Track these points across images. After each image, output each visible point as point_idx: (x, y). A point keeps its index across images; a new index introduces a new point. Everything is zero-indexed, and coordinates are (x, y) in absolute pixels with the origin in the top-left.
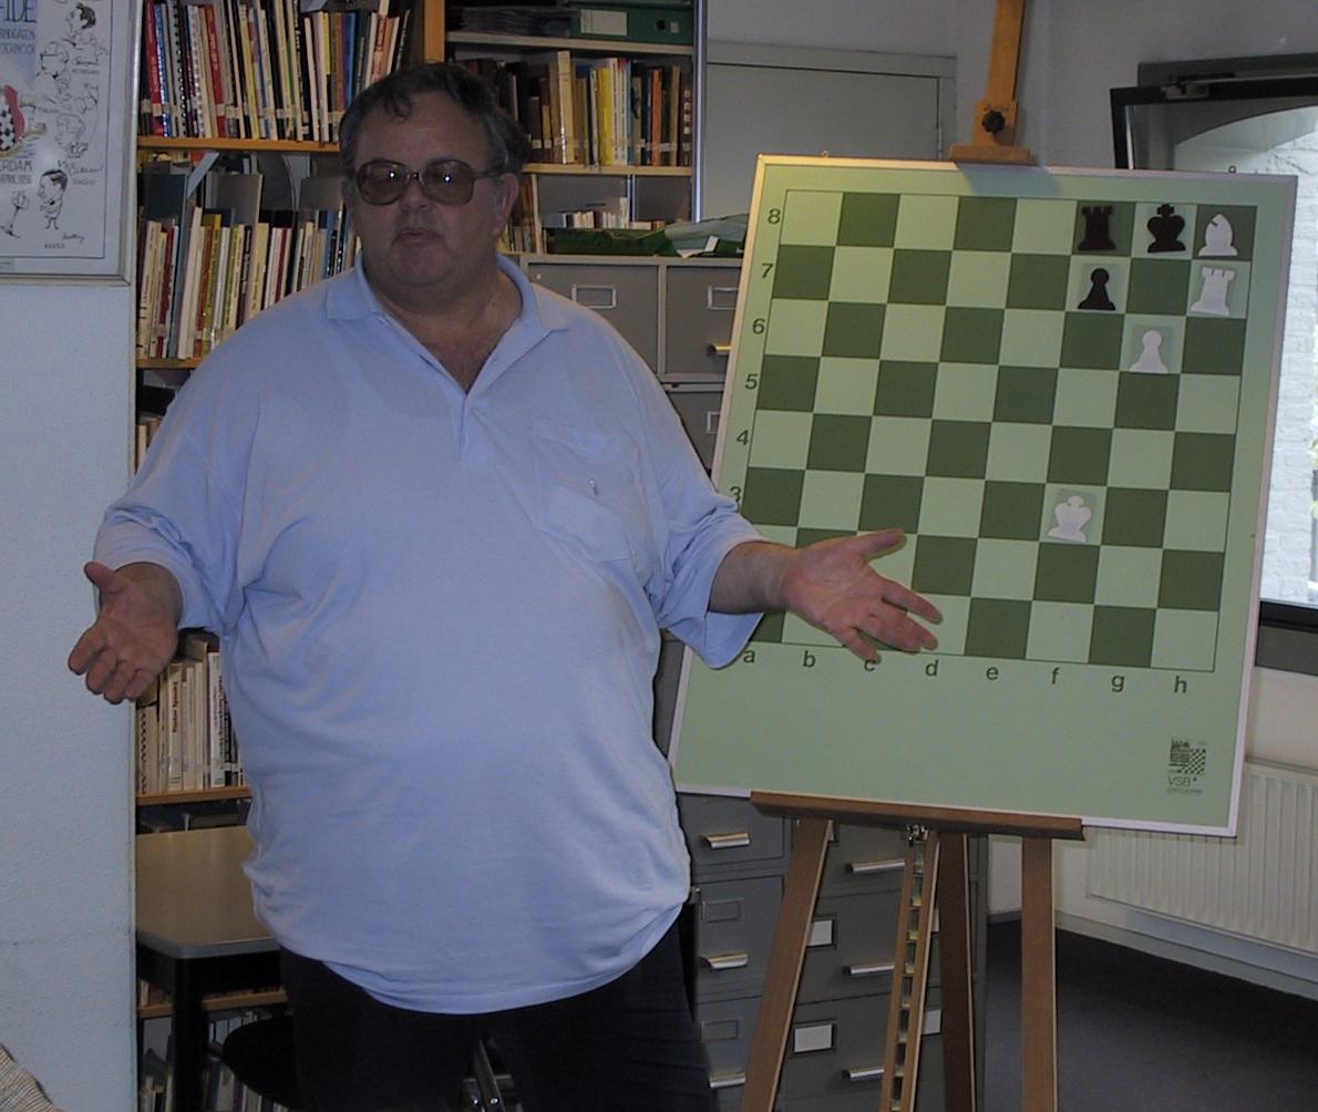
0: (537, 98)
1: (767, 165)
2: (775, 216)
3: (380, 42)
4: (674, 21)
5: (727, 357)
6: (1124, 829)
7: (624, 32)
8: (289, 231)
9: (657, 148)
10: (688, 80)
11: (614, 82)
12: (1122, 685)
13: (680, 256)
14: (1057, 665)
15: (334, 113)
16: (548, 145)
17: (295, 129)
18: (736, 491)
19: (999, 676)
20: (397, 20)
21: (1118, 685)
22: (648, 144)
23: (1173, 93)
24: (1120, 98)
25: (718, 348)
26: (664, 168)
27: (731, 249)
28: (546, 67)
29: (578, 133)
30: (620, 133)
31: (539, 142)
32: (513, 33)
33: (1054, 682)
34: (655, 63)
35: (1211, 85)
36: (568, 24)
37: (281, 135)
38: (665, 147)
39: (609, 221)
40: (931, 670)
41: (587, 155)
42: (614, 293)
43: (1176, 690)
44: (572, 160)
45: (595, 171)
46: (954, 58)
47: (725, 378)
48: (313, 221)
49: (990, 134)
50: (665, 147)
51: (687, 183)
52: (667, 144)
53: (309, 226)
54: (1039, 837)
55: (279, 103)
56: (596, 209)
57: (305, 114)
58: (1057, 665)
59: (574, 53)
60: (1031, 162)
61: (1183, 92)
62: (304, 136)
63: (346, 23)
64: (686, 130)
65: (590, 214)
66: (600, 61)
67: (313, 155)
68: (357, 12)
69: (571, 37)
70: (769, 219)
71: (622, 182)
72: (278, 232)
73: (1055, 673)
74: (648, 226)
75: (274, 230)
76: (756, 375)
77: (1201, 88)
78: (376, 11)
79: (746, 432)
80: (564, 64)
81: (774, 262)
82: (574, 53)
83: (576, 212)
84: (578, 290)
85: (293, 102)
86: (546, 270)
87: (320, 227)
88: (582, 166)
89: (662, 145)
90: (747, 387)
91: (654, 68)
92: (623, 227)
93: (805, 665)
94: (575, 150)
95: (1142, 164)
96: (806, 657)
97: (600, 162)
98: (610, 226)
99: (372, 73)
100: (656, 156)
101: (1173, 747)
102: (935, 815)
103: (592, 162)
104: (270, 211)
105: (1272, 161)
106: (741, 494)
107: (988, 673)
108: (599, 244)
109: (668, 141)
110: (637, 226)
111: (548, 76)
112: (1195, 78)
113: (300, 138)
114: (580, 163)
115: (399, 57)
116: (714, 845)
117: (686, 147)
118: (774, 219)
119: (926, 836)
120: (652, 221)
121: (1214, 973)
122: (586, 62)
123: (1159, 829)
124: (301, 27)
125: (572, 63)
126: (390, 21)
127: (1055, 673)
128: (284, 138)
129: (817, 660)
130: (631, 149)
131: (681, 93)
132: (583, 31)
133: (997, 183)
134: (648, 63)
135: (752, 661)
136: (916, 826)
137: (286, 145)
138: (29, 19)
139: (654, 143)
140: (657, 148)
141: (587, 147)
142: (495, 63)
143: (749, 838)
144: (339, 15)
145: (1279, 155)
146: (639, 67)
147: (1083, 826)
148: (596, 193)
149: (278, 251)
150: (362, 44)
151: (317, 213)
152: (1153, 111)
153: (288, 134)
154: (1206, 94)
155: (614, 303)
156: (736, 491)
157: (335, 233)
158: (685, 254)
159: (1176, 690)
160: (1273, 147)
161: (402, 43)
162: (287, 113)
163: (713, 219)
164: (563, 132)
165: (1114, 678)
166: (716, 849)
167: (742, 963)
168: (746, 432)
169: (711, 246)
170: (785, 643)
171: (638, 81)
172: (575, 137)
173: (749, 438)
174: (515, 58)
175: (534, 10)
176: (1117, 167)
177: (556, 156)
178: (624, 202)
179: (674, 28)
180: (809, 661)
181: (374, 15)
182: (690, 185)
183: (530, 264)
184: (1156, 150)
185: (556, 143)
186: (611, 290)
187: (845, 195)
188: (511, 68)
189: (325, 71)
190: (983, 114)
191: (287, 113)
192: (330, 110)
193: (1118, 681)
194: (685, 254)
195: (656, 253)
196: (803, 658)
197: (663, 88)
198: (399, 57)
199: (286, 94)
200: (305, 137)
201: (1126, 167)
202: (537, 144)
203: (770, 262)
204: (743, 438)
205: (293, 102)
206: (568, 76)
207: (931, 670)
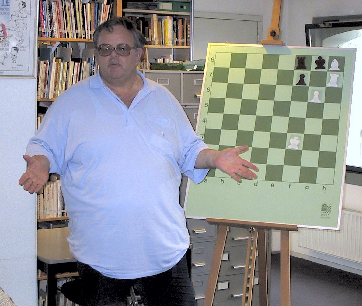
2: (213, 60)
8: (79, 64)
9: (180, 41)
10: (189, 22)
11: (169, 22)
12: (308, 189)
16: (150, 40)
18: (202, 135)
20: (109, 5)
22: (178, 40)
23: (322, 25)
24: (307, 27)
25: (197, 96)
27: (201, 69)
29: (159, 37)
30: (170, 36)
31: (148, 39)
32: (141, 9)
33: (289, 188)
35: (332, 24)
36: (156, 6)
37: (77, 37)
38: (183, 40)
39: (167, 61)
40: (256, 184)
41: (162, 43)
42: (169, 81)
43: (323, 190)
45: (164, 47)
46: (262, 16)
47: (199, 104)
49: (272, 37)
50: (183, 40)
51: (189, 50)
53: (85, 62)
54: (285, 230)
55: (77, 28)
56: (164, 57)
57: (84, 31)
59: (158, 15)
60: (283, 44)
62: (84, 37)
63: (95, 6)
65: (162, 59)
67: (86, 43)
68: (98, 3)
72: (76, 64)
74: (178, 62)
75: (75, 63)
76: (208, 103)
77: (330, 24)
79: (205, 119)
81: (213, 72)
83: (158, 58)
84: (159, 80)
85: (81, 28)
86: (150, 74)
87: (88, 62)
88: (160, 46)
94: (158, 41)
95: (314, 45)
96: (221, 181)
99: (102, 20)
100: (180, 43)
102: (257, 224)
103: (163, 45)
106: (204, 136)
110: (175, 62)
112: (328, 21)
113: (82, 38)
114: (159, 45)
116: (196, 233)
117: (188, 41)
118: (213, 60)
119: (254, 230)
122: (161, 16)
124: (83, 7)
125: (157, 17)
126: (107, 6)
129: (224, 181)
130: (173, 41)
132: (160, 9)
133: (274, 50)
134: (178, 17)
135: (207, 182)
137: (78, 40)
141: (161, 40)
144: (93, 4)
146: (176, 18)
147: (297, 227)
148: (164, 53)
150: (99, 12)
152: (317, 30)
153: (79, 37)
155: (169, 84)
157: (92, 64)
158: (188, 70)
159: (323, 190)
161: (110, 12)
163: (196, 60)
165: (306, 187)
166: (197, 234)
167: (204, 265)
168: (205, 119)
169: (195, 68)
170: (216, 177)
171: (175, 22)
172: (158, 38)
173: (206, 120)
174: (142, 16)
175: (147, 3)
176: (307, 46)
177: (153, 43)
178: (171, 55)
179: (185, 8)
180: (222, 182)
181: (103, 4)
184: (317, 42)
185: (153, 39)
186: (168, 80)
187: (232, 53)
188: (140, 18)
189: (89, 20)
190: (270, 31)
192: (91, 30)
193: (307, 187)
194: (188, 70)
196: (221, 181)
197: (182, 24)
200: (84, 38)
201: (309, 46)
204: (204, 120)
205: (81, 28)
207: (256, 184)
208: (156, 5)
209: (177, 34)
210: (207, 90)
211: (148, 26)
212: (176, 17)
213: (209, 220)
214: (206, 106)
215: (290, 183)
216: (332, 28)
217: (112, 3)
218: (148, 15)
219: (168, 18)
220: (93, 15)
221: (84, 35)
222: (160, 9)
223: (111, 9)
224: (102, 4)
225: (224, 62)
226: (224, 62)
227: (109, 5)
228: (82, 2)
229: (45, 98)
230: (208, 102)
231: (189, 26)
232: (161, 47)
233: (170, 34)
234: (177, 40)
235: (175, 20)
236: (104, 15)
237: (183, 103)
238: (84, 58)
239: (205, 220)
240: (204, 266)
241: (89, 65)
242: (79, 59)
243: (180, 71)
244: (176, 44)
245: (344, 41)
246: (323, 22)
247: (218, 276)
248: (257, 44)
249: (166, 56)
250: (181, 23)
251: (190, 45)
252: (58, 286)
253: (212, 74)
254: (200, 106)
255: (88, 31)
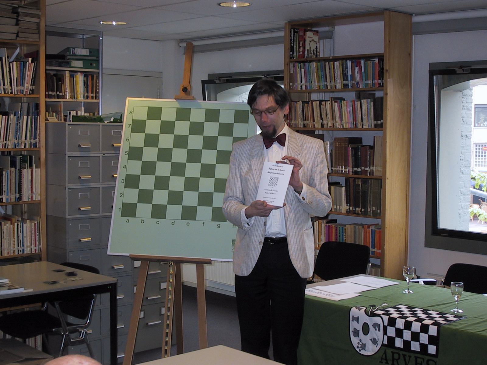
0: (60, 83)
1: (129, 100)
2: (131, 112)
3: (29, 69)
4: (94, 63)
5: (120, 147)
6: (218, 261)
7: (82, 66)
8: (7, 117)
9: (90, 95)
10: (98, 78)
11: (80, 79)
12: (220, 226)
13: (105, 122)
14: (204, 222)
15: (18, 87)
16: (63, 94)
17: (8, 91)
18: (123, 180)
19: (190, 225)
20: (33, 64)
21: (219, 226)
22: (88, 94)
23: (217, 81)
24: (204, 82)
25: (115, 145)
26: (92, 100)
27: (119, 120)
28: (63, 75)
29: (71, 92)
30: (81, 91)
31: (61, 93)
32: (55, 66)
33: (203, 226)
34: (90, 74)
35: (226, 79)
36: (68, 64)
37: (5, 93)
38: (92, 95)
39: (79, 114)
40: (173, 223)
41: (73, 96)
42: (89, 132)
43: (233, 227)
44: (69, 98)
45: (75, 101)
46: (162, 72)
47: (119, 152)
48: (13, 114)
49: (184, 92)
50: (92, 95)
51: (98, 104)
52: (93, 94)
53: (12, 115)
54: (201, 264)
55: (4, 85)
56: (76, 110)
57: (11, 87)
58: (204, 222)
59: (70, 71)
60: (194, 99)
61: (220, 81)
62: (11, 93)
63: (21, 64)
64: (98, 91)
65: (75, 112)
66: (77, 73)
67: (10, 97)
68: (23, 62)
69: (69, 67)
70: (130, 113)
71: (81, 103)
72: (4, 117)
73: (203, 223)
74: (88, 114)
75: (3, 116)
76: (127, 152)
77: (224, 80)
78: (28, 62)
79: (125, 166)
80: (67, 74)
81: (131, 124)
82: (70, 71)
83: (71, 111)
84: (80, 131)
85: (8, 84)
86: (71, 126)
87: (15, 116)
88: (72, 99)
89: (91, 94)
90: (125, 154)
91: (90, 75)
92: (83, 115)
93: (142, 223)
94: (70, 95)
95: (209, 100)
96: (142, 221)
97: (76, 98)
98: (80, 115)
99: (27, 77)
100: (90, 97)
101: (233, 241)
102: (175, 259)
103: (74, 99)
104: (2, 112)
105: (240, 98)
106: (124, 181)
107: (187, 224)
108: (84, 119)
109: (93, 93)
110: (86, 114)
111: (63, 77)
112: (223, 77)
113: (9, 93)
114: (71, 99)
115: (34, 73)
116: (115, 268)
117: (97, 95)
118: (131, 113)
119: (173, 264)
120: (89, 113)
121: (231, 296)
122: (73, 74)
123: (223, 261)
124: (9, 66)
125: (69, 74)
126: (32, 64)
127: (203, 223)
128: (5, 93)
129: (145, 221)
130: (84, 95)
131: (96, 82)
132: (72, 66)
133: (186, 104)
134: (88, 74)
135: (128, 222)
136: (170, 262)
137: (6, 95)
138: (157, 78)
139: (90, 94)
140: (90, 95)
141: (73, 95)
142: (50, 74)
143: (124, 266)
144: (19, 62)
145: (242, 96)
146: (86, 75)
147: (211, 261)
148: (76, 106)
149: (4, 121)
150: (25, 70)
151: (14, 112)
152: (212, 86)
153: (6, 92)
154: (226, 81)
155: (89, 134)
156: (123, 180)
157: (18, 117)
158: (106, 122)
159: (233, 227)
160: (240, 94)
161: (35, 70)
162: (6, 87)
163: (113, 113)
164: (67, 90)
165: (218, 225)
166: (116, 269)
167: (123, 297)
168: (125, 166)
169: (112, 120)
170: (137, 217)
171: (86, 78)
172: (70, 92)
173: (126, 167)
174: (55, 73)
175: (60, 60)
176: (203, 100)
177: (66, 97)
178: (83, 108)
179: (94, 65)
180: (143, 222)
181: (28, 63)
182: (99, 104)
183: (68, 125)
184: (212, 96)
185: (65, 94)
186: (88, 131)
187: (149, 107)
188: (54, 75)
189: (15, 77)
190: (182, 88)
191: (6, 87)
192: (17, 86)
193: (219, 225)
194: (106, 122)
195: (99, 122)
196: (141, 221)
197: (92, 80)
198: (34, 73)
199: (6, 82)
200: (11, 93)
201: (206, 100)
202: (61, 94)
203: (130, 124)
204: (124, 167)
205: (8, 84)
206: (68, 77)
207: (173, 223)
208: (68, 63)
209: (87, 89)
210: (127, 139)
211: (61, 81)
212: (86, 73)
213: (132, 257)
214: (126, 154)
215: (203, 222)
216: (226, 84)
217: (36, 62)
218: (62, 72)
219: (79, 74)
220: (19, 72)
221: (11, 91)
222: (72, 66)
223: (35, 67)
224: (27, 62)
225: (142, 115)
226: (142, 115)
227: (33, 64)
228: (9, 61)
229: (7, 147)
230: (128, 151)
231: (97, 81)
232: (73, 101)
233: (81, 88)
234: (322, 122)
235: (85, 76)
236: (29, 72)
237: (102, 151)
238: (11, 112)
239: (129, 256)
240: (122, 298)
241: (16, 118)
242: (7, 112)
243: (98, 123)
244: (86, 98)
245: (235, 94)
246: (218, 78)
247: (142, 306)
248: (158, 98)
249: (78, 108)
250: (91, 79)
251: (99, 99)
252: (438, 227)
253: (131, 126)
254: (120, 154)
255: (14, 87)
